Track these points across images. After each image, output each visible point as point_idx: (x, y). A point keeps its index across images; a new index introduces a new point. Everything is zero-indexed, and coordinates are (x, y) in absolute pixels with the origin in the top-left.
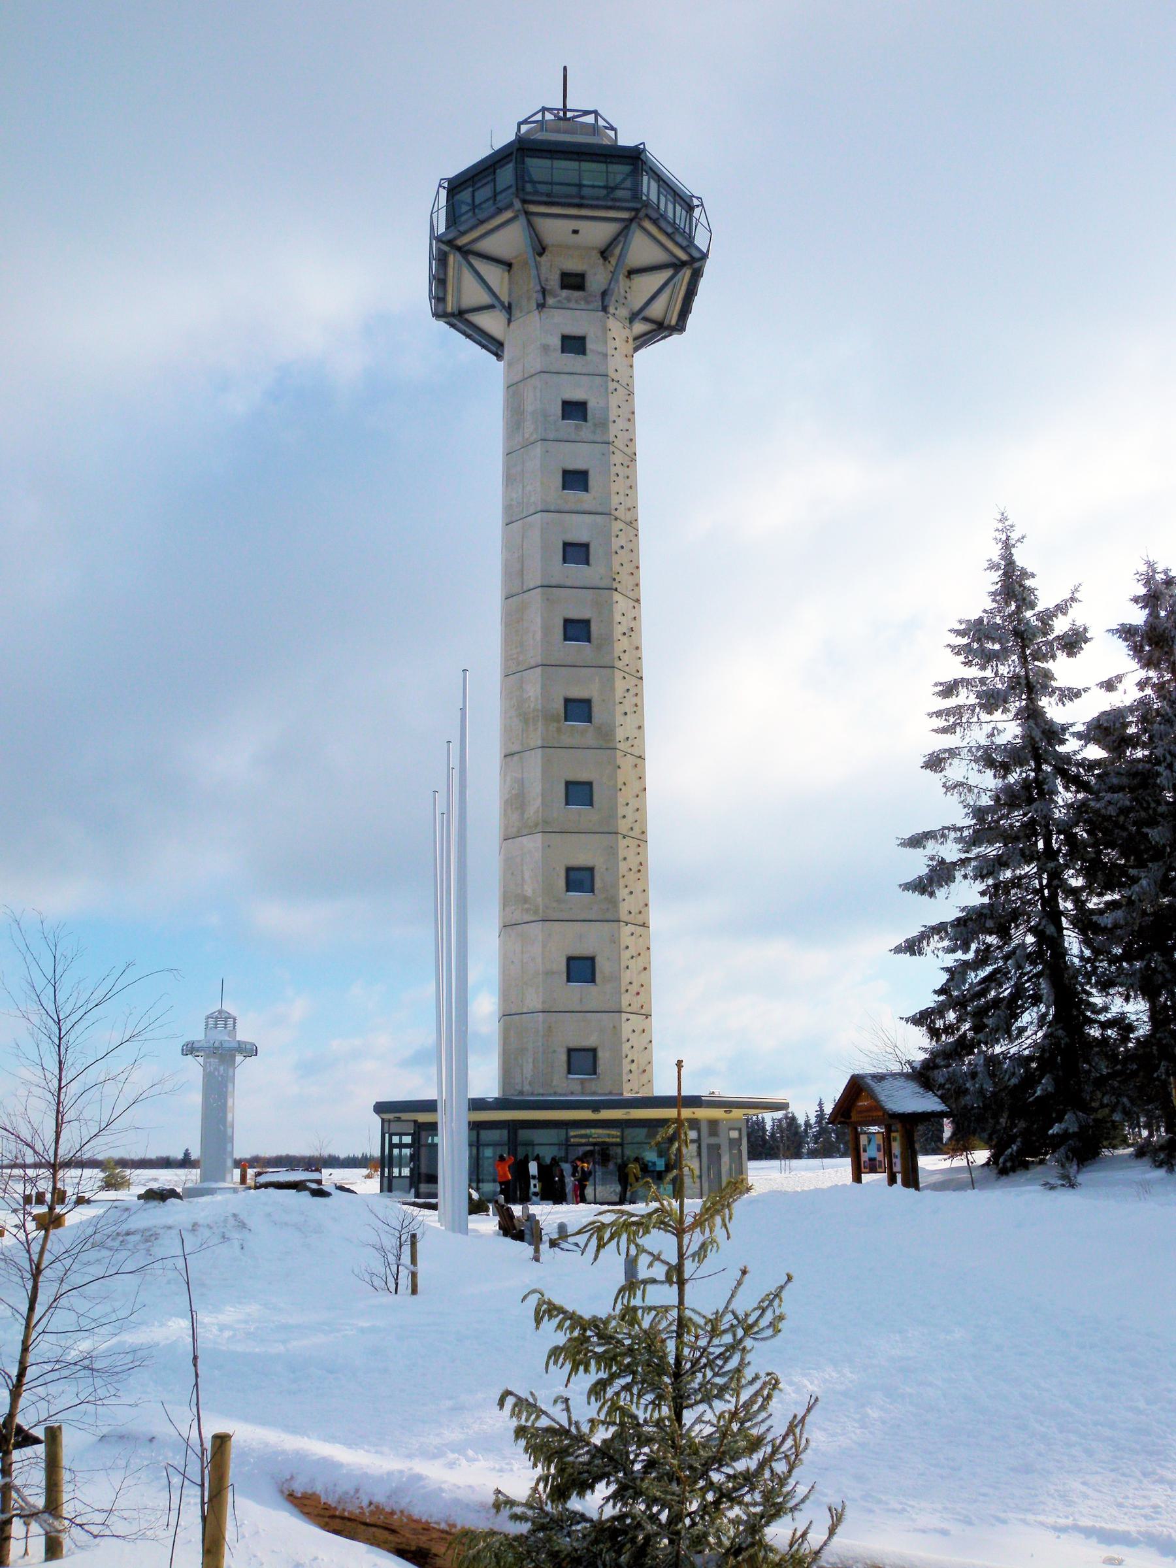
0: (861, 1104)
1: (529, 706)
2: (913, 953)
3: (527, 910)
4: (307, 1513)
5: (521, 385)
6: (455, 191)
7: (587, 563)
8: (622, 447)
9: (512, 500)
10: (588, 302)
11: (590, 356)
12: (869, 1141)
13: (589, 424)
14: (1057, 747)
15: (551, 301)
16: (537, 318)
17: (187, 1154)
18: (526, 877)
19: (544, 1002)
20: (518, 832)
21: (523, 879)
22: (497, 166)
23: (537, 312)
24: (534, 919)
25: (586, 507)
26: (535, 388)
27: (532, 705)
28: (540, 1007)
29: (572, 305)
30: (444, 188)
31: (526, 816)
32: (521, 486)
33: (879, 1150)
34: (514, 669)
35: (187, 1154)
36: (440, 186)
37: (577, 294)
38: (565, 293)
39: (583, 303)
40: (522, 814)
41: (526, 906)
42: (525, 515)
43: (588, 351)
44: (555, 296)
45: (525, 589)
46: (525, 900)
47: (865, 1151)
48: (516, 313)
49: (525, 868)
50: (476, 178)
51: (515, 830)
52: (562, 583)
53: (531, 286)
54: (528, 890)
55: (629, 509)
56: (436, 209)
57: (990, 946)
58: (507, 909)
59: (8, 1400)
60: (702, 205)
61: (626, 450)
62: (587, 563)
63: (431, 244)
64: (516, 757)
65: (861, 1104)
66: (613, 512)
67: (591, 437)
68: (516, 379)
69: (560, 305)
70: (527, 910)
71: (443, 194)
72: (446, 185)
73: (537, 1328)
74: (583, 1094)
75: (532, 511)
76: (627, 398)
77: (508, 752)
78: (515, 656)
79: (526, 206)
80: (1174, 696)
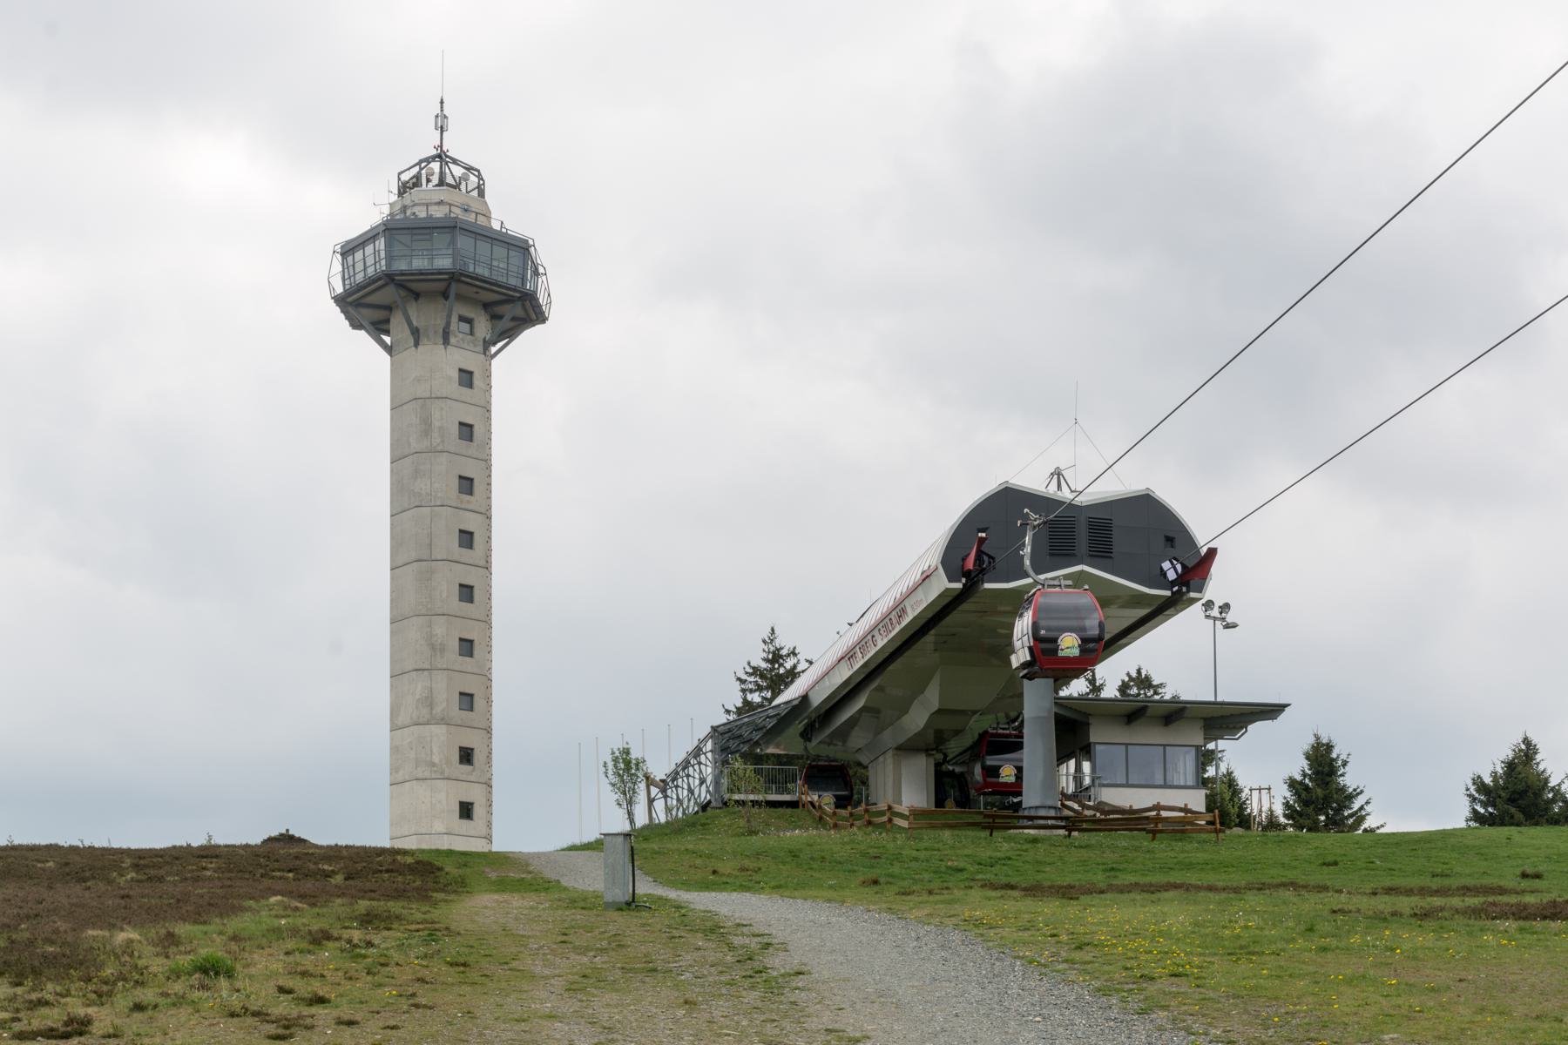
1: (437, 641)
2: (1148, 678)
3: (435, 772)
4: (779, 887)
10: (475, 346)
11: (476, 390)
14: (1014, 667)
15: (453, 340)
16: (443, 351)
18: (434, 751)
21: (431, 751)
22: (366, 243)
24: (440, 777)
25: (470, 507)
26: (442, 409)
27: (439, 641)
28: (444, 831)
29: (465, 346)
31: (434, 712)
39: (471, 345)
40: (432, 709)
41: (435, 769)
44: (456, 336)
45: (433, 558)
46: (433, 765)
48: (423, 340)
51: (425, 720)
54: (436, 759)
58: (419, 769)
64: (426, 673)
70: (435, 772)
73: (1289, 705)
74: (1097, 609)
75: (438, 503)
80: (146, 1041)
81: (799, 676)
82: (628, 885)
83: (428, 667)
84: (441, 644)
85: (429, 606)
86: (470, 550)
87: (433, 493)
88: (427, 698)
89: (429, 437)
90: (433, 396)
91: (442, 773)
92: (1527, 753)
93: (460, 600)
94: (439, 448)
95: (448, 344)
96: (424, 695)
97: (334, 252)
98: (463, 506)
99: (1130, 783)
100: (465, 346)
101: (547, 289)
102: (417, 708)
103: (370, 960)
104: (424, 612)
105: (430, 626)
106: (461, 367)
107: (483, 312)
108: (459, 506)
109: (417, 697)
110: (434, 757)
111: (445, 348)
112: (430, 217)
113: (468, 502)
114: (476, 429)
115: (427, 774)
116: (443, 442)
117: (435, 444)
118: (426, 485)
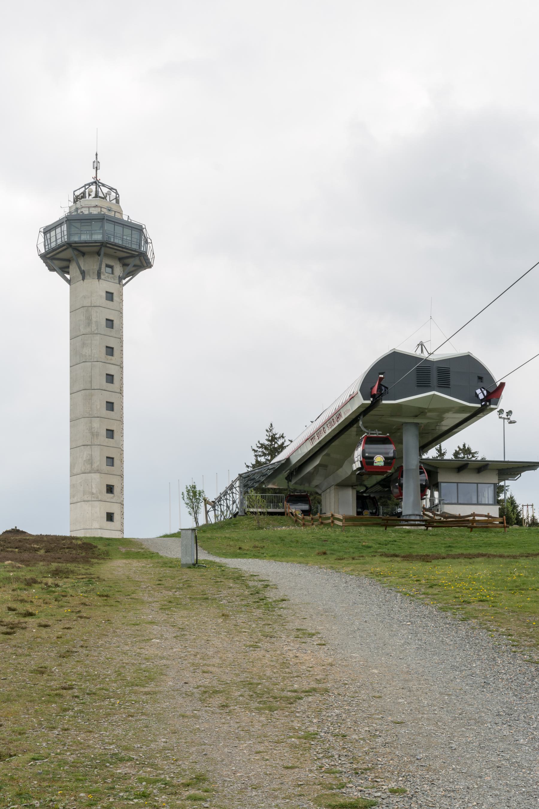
0: (384, 402)
1: (94, 430)
3: (94, 497)
4: (274, 556)
5: (90, 308)
10: (114, 279)
13: (114, 330)
15: (102, 277)
16: (98, 282)
19: (200, 560)
25: (112, 362)
27: (96, 430)
29: (109, 280)
31: (93, 467)
39: (112, 279)
40: (92, 466)
42: (92, 361)
44: (104, 275)
45: (92, 388)
46: (93, 494)
48: (87, 277)
49: (93, 483)
52: (106, 389)
53: (95, 267)
54: (94, 491)
57: (534, 575)
64: (89, 447)
65: (384, 402)
67: (115, 336)
69: (105, 279)
75: (95, 360)
83: (90, 444)
84: (96, 432)
85: (91, 413)
86: (111, 302)
87: (92, 355)
88: (89, 460)
89: (90, 326)
90: (92, 305)
91: (97, 498)
93: (107, 410)
95: (100, 279)
97: (40, 232)
101: (152, 250)
102: (84, 464)
104: (88, 415)
105: (91, 423)
107: (118, 262)
109: (84, 459)
110: (93, 490)
111: (99, 281)
113: (111, 360)
114: (115, 322)
115: (89, 499)
116: (97, 329)
117: (93, 330)
118: (89, 351)
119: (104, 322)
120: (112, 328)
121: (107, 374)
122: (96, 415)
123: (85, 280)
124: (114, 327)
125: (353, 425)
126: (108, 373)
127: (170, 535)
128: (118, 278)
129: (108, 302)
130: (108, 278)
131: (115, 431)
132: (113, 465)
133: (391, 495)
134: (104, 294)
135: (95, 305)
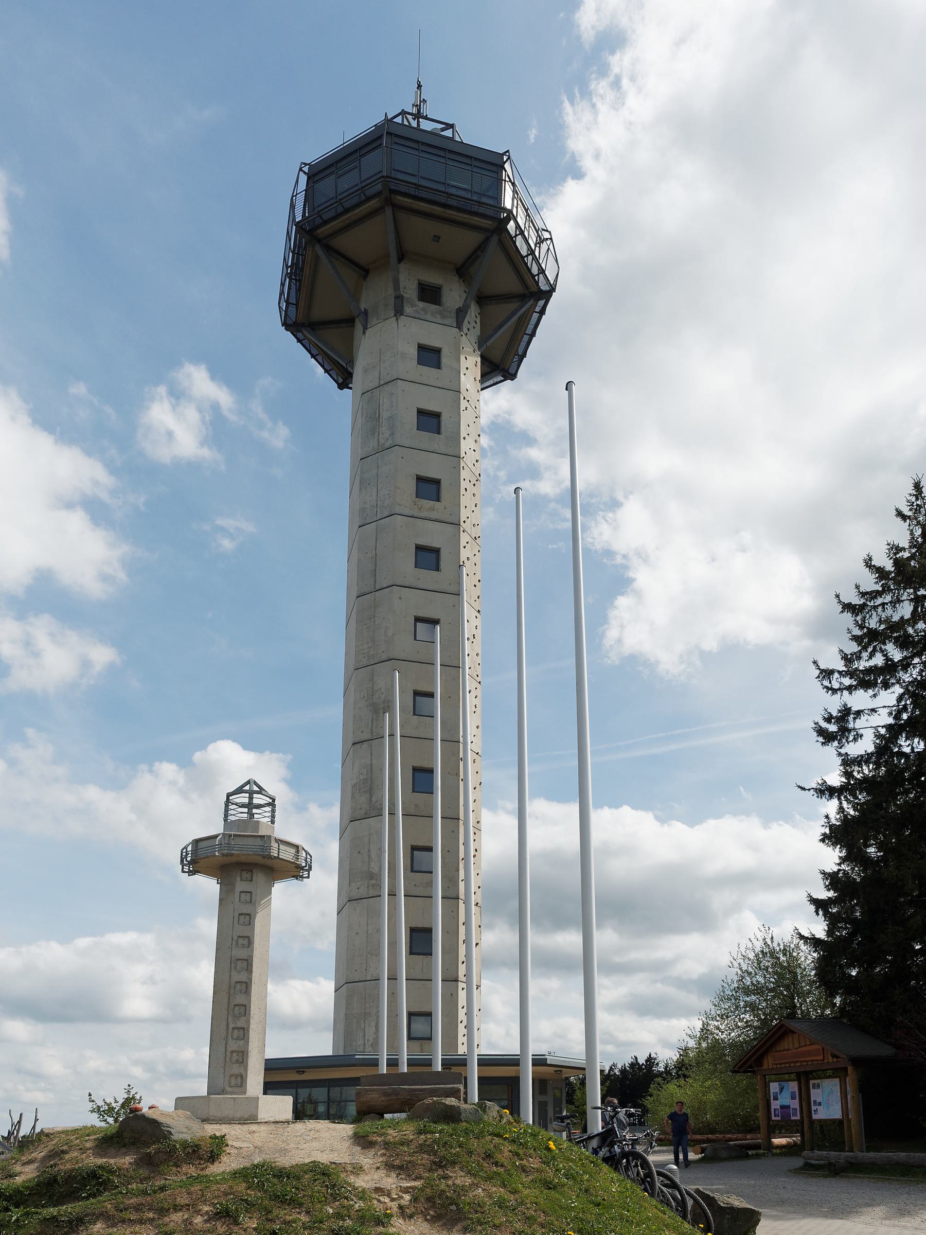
5: (377, 392)
6: (316, 178)
7: (437, 569)
8: (471, 465)
9: (366, 503)
10: (443, 317)
12: (782, 1089)
15: (408, 310)
17: (850, 693)
20: (366, 813)
21: (369, 856)
23: (394, 318)
25: (433, 515)
27: (383, 697)
29: (428, 317)
30: (305, 173)
31: (374, 799)
32: (375, 490)
33: (793, 1098)
34: (365, 662)
35: (850, 693)
36: (301, 170)
37: (434, 307)
38: (421, 304)
39: (439, 316)
40: (371, 796)
43: (443, 365)
44: (413, 305)
45: (378, 588)
47: (776, 1099)
48: (373, 321)
50: (339, 165)
51: (363, 812)
55: (474, 525)
56: (295, 194)
58: (353, 884)
59: (295, 311)
60: (551, 239)
61: (473, 468)
62: (437, 569)
63: (283, 284)
64: (365, 745)
66: (462, 523)
67: (443, 450)
68: (372, 385)
69: (417, 316)
71: (303, 179)
72: (306, 169)
76: (475, 420)
77: (357, 740)
78: (366, 651)
79: (393, 196)
81: (897, 700)
82: (477, 1037)
83: (369, 736)
84: (384, 703)
86: (434, 573)
92: (823, 873)
94: (388, 444)
96: (362, 777)
98: (422, 515)
99: (413, 952)
100: (428, 317)
103: (394, 1230)
105: (372, 679)
106: (422, 342)
107: (456, 278)
108: (416, 514)
110: (372, 864)
111: (397, 319)
112: (418, 128)
113: (432, 509)
114: (444, 418)
116: (392, 434)
119: (412, 418)
120: (439, 432)
121: (419, 548)
122: (384, 657)
123: (368, 332)
124: (443, 429)
125: (70, 1177)
126: (422, 542)
127: (781, 1146)
128: (454, 315)
129: (425, 370)
130: (426, 312)
131: (442, 482)
132: (438, 499)
133: (360, 1148)
134: (414, 352)
135: (389, 379)
